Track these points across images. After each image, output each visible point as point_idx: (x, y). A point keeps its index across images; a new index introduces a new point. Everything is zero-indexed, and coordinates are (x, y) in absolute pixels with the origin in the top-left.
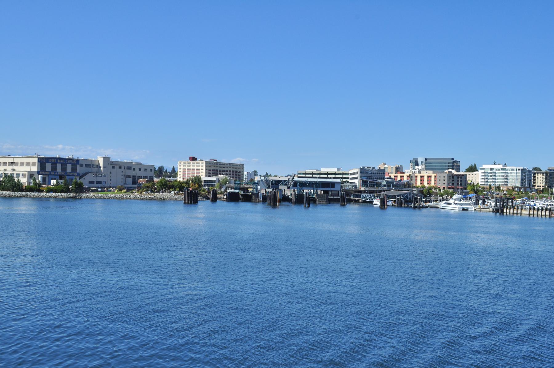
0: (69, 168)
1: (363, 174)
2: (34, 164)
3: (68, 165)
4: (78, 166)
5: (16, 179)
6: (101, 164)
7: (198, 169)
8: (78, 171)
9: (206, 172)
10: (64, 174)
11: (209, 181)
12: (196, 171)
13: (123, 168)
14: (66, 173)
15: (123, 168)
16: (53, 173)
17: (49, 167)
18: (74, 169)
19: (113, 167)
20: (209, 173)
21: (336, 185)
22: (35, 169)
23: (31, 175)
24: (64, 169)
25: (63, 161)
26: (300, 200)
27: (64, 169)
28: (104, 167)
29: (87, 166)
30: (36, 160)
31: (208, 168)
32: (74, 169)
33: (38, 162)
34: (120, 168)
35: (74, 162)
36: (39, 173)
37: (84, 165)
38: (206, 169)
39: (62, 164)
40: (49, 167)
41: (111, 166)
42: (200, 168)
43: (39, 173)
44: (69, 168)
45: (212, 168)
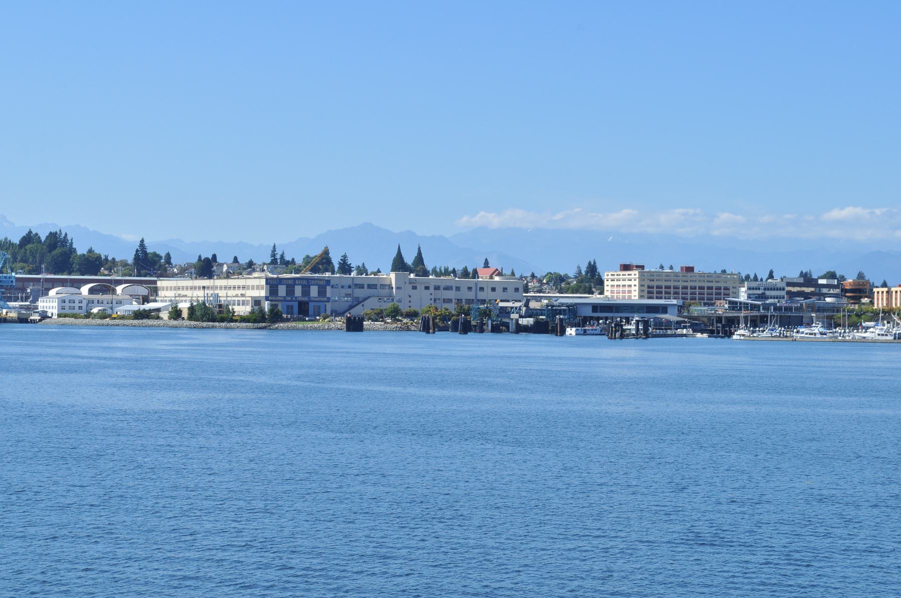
0: (314, 291)
1: (751, 292)
2: (262, 288)
3: (296, 287)
4: (328, 288)
5: (230, 307)
6: (394, 286)
7: (630, 286)
8: (328, 295)
9: (641, 291)
10: (306, 299)
11: (755, 305)
12: (689, 291)
13: (432, 288)
14: (309, 298)
15: (432, 288)
16: (289, 299)
17: (282, 290)
18: (322, 292)
19: (414, 288)
20: (649, 292)
21: (669, 310)
22: (263, 293)
23: (257, 302)
24: (306, 292)
25: (304, 282)
26: (540, 328)
27: (306, 292)
28: (397, 288)
29: (369, 286)
30: (263, 282)
31: (647, 283)
32: (322, 292)
33: (267, 283)
34: (427, 288)
35: (322, 283)
36: (267, 298)
37: (366, 286)
38: (641, 286)
39: (303, 286)
40: (282, 290)
41: (411, 286)
42: (632, 283)
43: (267, 298)
44: (314, 291)
45: (655, 284)
